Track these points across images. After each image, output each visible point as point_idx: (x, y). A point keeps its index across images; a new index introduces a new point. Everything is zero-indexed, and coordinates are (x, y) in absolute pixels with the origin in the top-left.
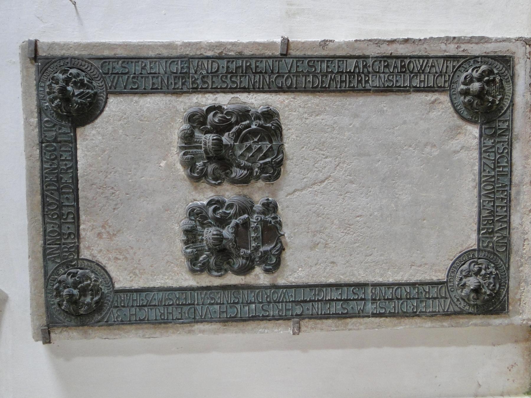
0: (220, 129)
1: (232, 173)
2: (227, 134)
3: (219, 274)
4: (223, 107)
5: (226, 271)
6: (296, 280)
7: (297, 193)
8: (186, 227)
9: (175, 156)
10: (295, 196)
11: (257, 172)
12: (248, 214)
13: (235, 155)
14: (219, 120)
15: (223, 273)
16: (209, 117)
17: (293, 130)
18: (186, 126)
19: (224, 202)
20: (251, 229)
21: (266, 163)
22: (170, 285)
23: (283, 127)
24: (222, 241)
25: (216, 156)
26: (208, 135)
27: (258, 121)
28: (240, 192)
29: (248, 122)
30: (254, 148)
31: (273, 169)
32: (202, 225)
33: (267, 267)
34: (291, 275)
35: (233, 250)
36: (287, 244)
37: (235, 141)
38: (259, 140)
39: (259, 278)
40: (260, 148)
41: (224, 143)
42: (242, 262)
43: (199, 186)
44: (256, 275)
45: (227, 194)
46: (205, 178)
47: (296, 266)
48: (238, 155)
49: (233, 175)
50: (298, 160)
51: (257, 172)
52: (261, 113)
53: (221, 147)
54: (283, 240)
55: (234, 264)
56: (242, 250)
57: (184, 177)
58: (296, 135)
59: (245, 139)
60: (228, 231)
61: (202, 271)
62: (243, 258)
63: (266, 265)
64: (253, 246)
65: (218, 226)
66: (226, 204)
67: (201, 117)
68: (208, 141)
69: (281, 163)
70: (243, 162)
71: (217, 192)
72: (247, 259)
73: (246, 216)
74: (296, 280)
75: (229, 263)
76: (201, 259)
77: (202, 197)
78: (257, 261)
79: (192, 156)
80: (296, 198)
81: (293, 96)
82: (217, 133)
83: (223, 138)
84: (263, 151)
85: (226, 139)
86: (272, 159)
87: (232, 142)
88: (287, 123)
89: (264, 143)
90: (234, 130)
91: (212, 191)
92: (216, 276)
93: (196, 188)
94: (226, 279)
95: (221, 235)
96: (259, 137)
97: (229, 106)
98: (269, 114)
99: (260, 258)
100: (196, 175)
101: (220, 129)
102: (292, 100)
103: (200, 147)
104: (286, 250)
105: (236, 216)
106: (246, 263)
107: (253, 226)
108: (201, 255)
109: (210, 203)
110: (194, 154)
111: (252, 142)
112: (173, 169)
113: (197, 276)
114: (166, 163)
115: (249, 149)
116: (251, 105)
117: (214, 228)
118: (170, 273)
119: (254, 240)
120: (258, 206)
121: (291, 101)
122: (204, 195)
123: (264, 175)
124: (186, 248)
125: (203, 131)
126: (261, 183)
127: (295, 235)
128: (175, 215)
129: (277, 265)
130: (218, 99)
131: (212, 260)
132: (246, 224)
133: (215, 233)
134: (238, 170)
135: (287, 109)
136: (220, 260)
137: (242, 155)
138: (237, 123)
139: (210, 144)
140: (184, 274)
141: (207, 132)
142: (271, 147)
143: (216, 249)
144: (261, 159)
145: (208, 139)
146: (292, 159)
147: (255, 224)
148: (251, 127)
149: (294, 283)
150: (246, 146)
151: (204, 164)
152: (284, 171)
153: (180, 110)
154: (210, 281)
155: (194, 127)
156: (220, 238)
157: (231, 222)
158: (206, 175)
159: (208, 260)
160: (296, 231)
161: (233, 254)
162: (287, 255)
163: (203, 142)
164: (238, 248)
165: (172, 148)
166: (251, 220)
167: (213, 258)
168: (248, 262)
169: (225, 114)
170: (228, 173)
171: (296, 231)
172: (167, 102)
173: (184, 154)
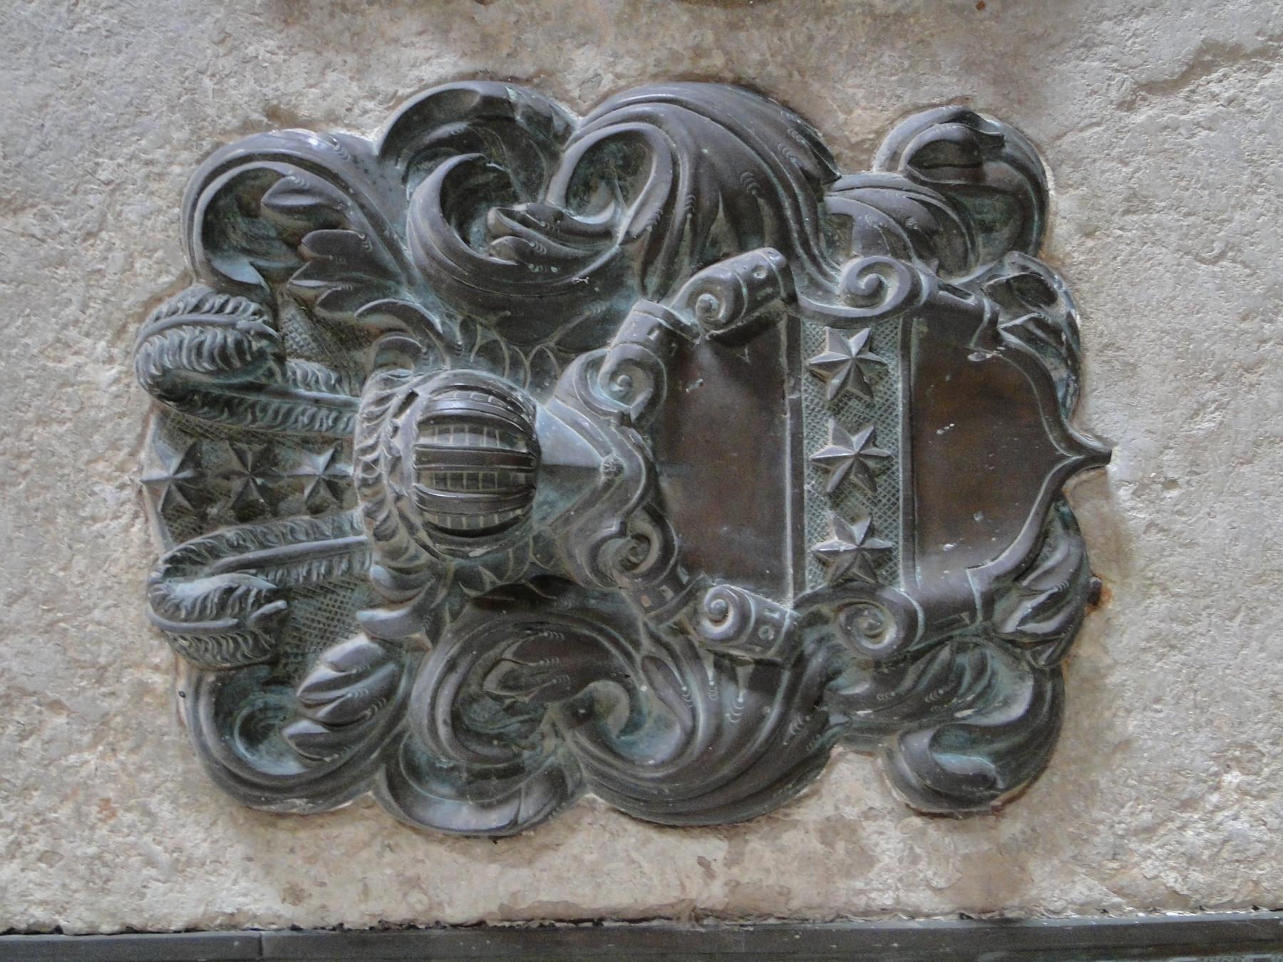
3: (496, 819)
5: (560, 789)
6: (1197, 876)
7: (1224, 83)
8: (172, 349)
10: (1203, 111)
12: (784, 245)
15: (527, 808)
19: (545, 134)
20: (804, 392)
22: (40, 915)
24: (524, 495)
32: (341, 343)
33: (954, 762)
34: (1148, 831)
35: (629, 596)
36: (1120, 551)
39: (864, 859)
42: (717, 712)
44: (832, 829)
45: (585, 61)
47: (1197, 752)
54: (1084, 514)
55: (633, 725)
56: (718, 593)
60: (589, 405)
61: (324, 786)
62: (726, 667)
63: (935, 741)
64: (824, 560)
65: (490, 354)
66: (571, 153)
71: (487, 42)
72: (763, 678)
73: (765, 257)
74: (1197, 876)
75: (586, 716)
76: (321, 671)
77: (341, 87)
78: (851, 703)
91: (443, 31)
92: (470, 836)
94: (555, 859)
95: (513, 424)
99: (889, 669)
104: (1111, 606)
105: (663, 253)
106: (751, 725)
107: (828, 354)
108: (328, 638)
109: (411, 135)
113: (283, 836)
117: (447, 372)
118: (37, 798)
119: (837, 497)
120: (873, 184)
122: (360, 73)
124: (178, 567)
127: (1194, 468)
128: (91, 254)
129: (1030, 747)
131: (428, 685)
132: (756, 342)
133: (453, 404)
136: (510, 682)
140: (165, 811)
143: (465, 578)
147: (855, 342)
149: (1178, 899)
154: (414, 883)
156: (513, 468)
157: (611, 321)
159: (388, 691)
160: (1206, 424)
161: (624, 625)
162: (1126, 651)
164: (679, 571)
166: (808, 302)
167: (433, 665)
168: (773, 713)
171: (1206, 424)
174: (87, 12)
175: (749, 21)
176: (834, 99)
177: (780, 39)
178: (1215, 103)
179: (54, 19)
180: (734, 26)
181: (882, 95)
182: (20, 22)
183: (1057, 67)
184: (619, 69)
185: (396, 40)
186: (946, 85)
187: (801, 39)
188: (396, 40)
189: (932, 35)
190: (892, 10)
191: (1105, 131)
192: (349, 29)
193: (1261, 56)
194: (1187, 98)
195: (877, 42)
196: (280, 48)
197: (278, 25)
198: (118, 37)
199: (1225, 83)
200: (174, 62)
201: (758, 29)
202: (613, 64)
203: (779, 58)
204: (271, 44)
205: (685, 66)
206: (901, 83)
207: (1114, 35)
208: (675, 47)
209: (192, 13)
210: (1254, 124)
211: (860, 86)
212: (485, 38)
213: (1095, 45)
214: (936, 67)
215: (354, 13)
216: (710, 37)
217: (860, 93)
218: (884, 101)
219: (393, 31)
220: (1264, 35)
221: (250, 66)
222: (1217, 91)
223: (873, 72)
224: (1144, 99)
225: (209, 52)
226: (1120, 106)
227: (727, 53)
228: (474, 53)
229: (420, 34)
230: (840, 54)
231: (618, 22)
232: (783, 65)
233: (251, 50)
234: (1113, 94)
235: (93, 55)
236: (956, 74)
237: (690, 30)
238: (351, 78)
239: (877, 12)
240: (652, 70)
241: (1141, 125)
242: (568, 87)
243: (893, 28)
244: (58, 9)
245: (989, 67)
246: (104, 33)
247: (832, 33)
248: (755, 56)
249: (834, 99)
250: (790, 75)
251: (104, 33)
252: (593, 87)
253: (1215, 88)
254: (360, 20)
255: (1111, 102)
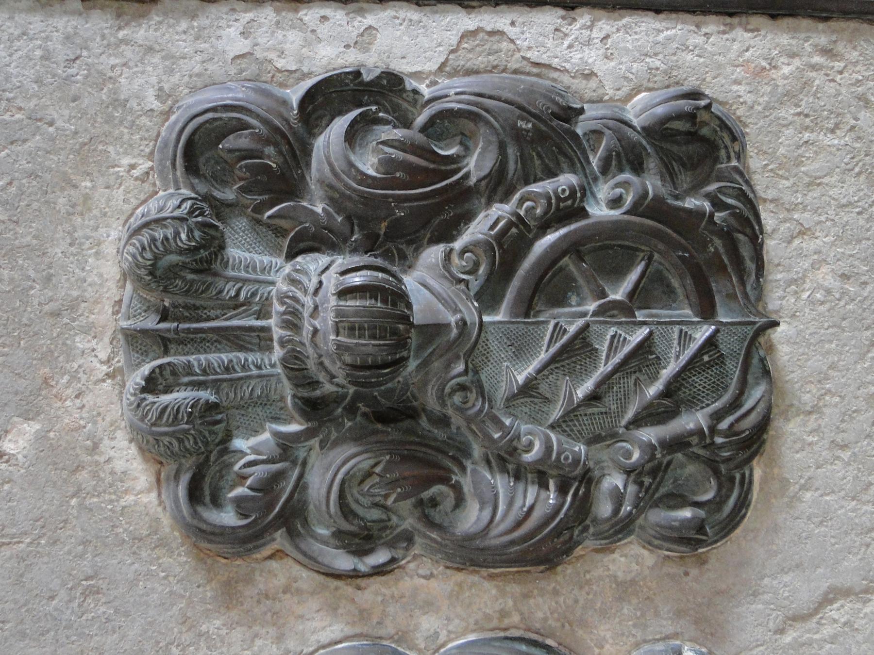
0: (402, 215)
1: (460, 501)
2: (434, 254)
4: (411, 84)
9: (98, 393)
11: (618, 498)
13: (481, 393)
14: (388, 164)
16: (319, 143)
17: (822, 240)
18: (170, 198)
21: (677, 444)
23: (768, 220)
25: (357, 397)
26: (312, 263)
27: (627, 176)
28: (503, 614)
29: (567, 180)
30: (604, 348)
31: (717, 473)
37: (488, 297)
38: (640, 296)
40: (645, 347)
41: (418, 318)
43: (248, 580)
45: (428, 624)
46: (292, 534)
48: (501, 393)
49: (472, 517)
50: (848, 415)
51: (618, 498)
52: (647, 131)
53: (402, 343)
57: (155, 526)
58: (843, 267)
59: (549, 288)
67: (268, 142)
68: (308, 301)
69: (754, 441)
70: (536, 441)
71: (363, 615)
79: (206, 395)
80: (833, 639)
81: (823, 41)
82: (370, 245)
83: (410, 282)
84: (658, 363)
85: (428, 282)
86: (717, 416)
87: (470, 311)
88: (787, 198)
89: (664, 314)
90: (479, 228)
91: (333, 609)
93: (229, 594)
96: (633, 276)
97: (444, 82)
98: (693, 136)
100: (228, 518)
101: (402, 215)
102: (817, 59)
103: (261, 339)
110: (216, 385)
111: (592, 306)
112: (83, 475)
114: (41, 437)
115: (575, 352)
116: (578, 84)
121: (814, 67)
123: (658, 516)
125: (280, 232)
126: (631, 559)
130: (382, 40)
134: (501, 483)
135: (787, 112)
137: (528, 389)
138: (498, 185)
139: (327, 320)
141: (305, 243)
142: (710, 343)
144: (651, 415)
145: (309, 291)
146: (815, 410)
148: (582, 213)
150: (559, 331)
151: (286, 447)
152: (764, 480)
153: (140, 98)
155: (221, 209)
158: (293, 518)
163: (278, 307)
165: (81, 343)
169: (424, 129)
170: (434, 503)
172: (56, 45)
173: (151, 385)
174: (92, 606)
175: (536, 592)
176: (592, 640)
177: (557, 603)
178: (836, 625)
179: (69, 611)
180: (526, 596)
181: (623, 634)
182: (46, 615)
183: (736, 610)
184: (451, 628)
185: (302, 617)
186: (664, 626)
187: (570, 602)
188: (302, 617)
189: (655, 594)
190: (628, 578)
191: (766, 649)
192: (270, 611)
193: (862, 593)
194: (818, 623)
195: (620, 599)
196: (224, 625)
197: (223, 610)
198: (113, 623)
199: (842, 610)
200: (151, 638)
201: (542, 596)
202: (447, 625)
203: (556, 615)
204: (218, 623)
205: (495, 623)
206: (635, 626)
207: (772, 587)
208: (488, 611)
209: (163, 604)
210: (860, 637)
211: (609, 630)
212: (362, 611)
213: (759, 594)
214: (657, 614)
215: (274, 599)
216: (510, 603)
217: (608, 635)
218: (624, 638)
219: (300, 610)
220: (867, 580)
221: (203, 639)
222: (836, 617)
223: (617, 620)
224: (791, 625)
225: (176, 630)
226: (775, 632)
227: (522, 614)
228: (354, 622)
229: (318, 611)
230: (595, 610)
231: (450, 597)
232: (558, 620)
233: (204, 628)
234: (771, 625)
235: (96, 635)
236: (670, 618)
237: (497, 600)
238: (272, 643)
239: (619, 580)
240: (472, 627)
241: (789, 644)
242: (417, 642)
243: (630, 590)
244: (71, 605)
245: (692, 612)
246: (104, 621)
247: (591, 596)
248: (540, 615)
249: (592, 640)
250: (563, 626)
251: (104, 621)
252: (433, 641)
253: (835, 614)
254: (278, 605)
255: (770, 631)
